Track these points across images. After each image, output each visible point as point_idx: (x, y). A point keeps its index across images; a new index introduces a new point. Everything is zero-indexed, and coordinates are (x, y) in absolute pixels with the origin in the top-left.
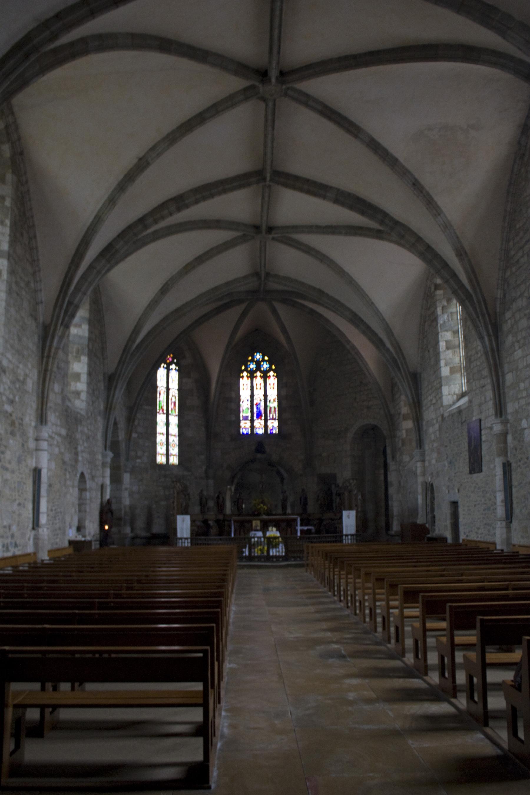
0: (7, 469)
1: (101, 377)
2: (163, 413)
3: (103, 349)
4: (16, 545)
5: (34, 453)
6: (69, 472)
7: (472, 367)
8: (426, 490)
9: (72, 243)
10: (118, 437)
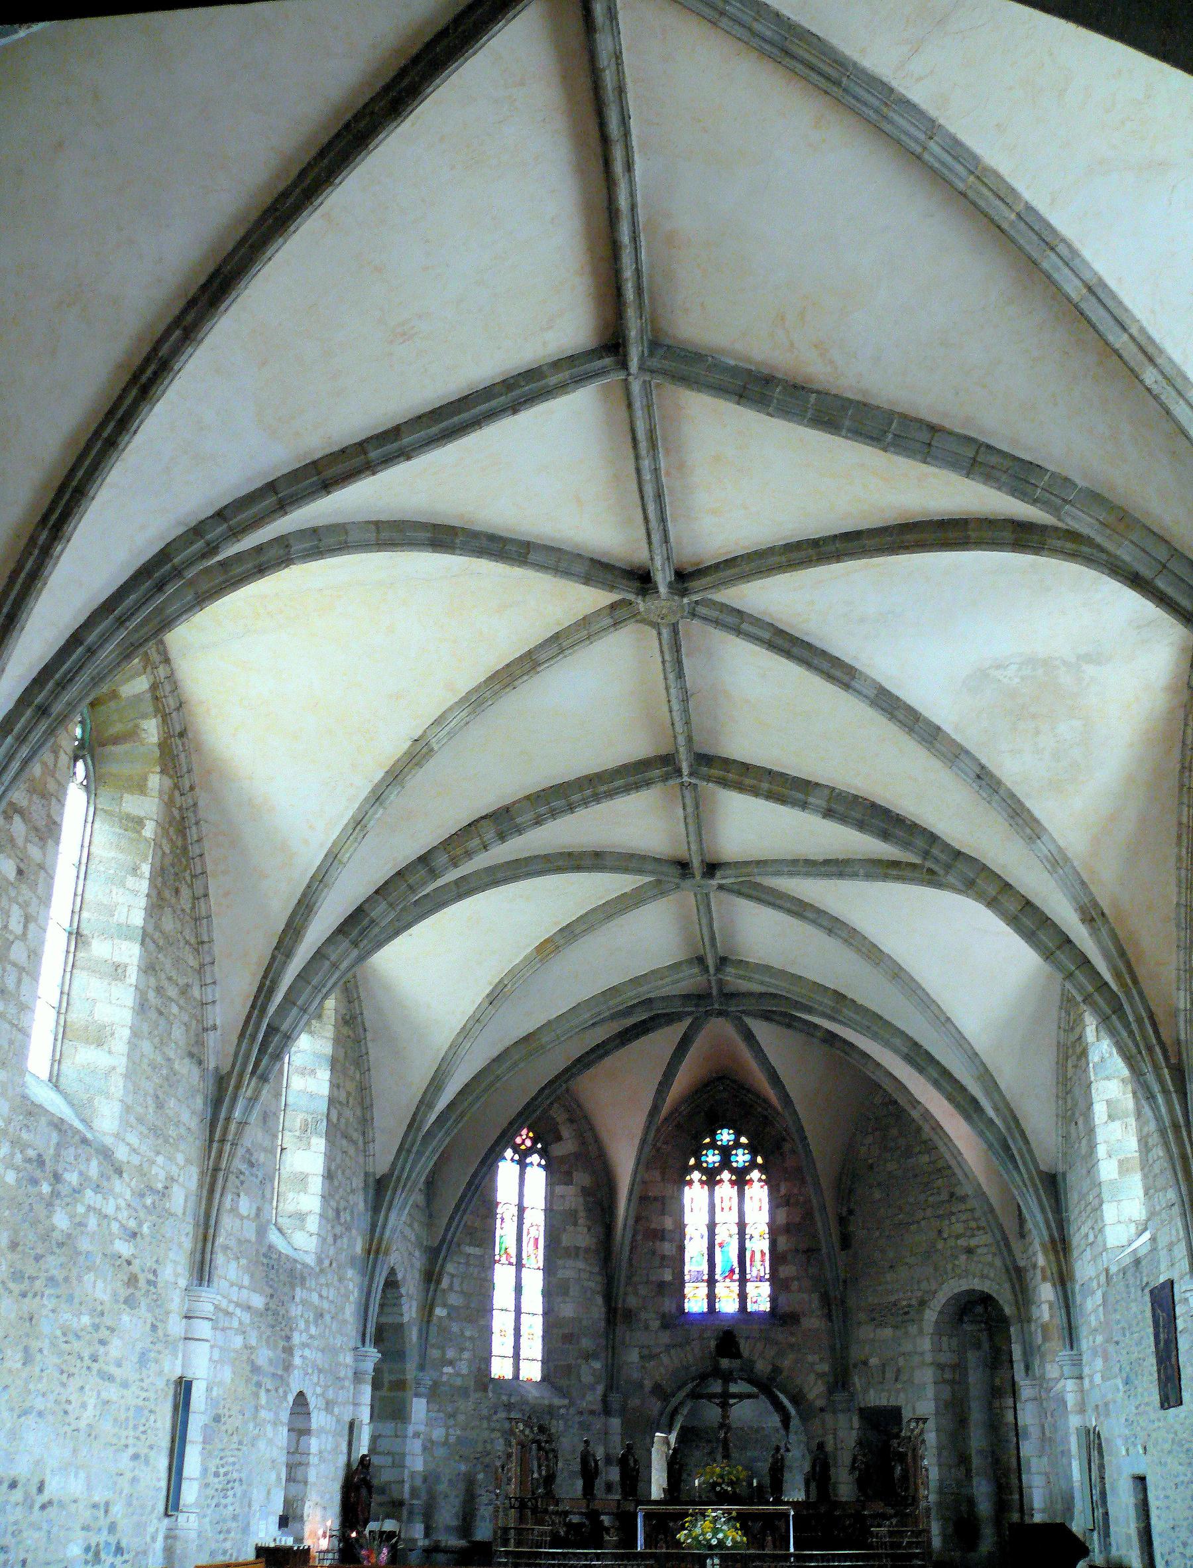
0: (110, 1378)
1: (358, 1182)
2: (510, 1264)
3: (365, 1122)
4: (119, 1550)
5: (181, 1345)
6: (268, 1391)
7: (1151, 1161)
8: (1089, 1448)
9: (280, 910)
10: (402, 1315)
